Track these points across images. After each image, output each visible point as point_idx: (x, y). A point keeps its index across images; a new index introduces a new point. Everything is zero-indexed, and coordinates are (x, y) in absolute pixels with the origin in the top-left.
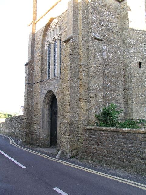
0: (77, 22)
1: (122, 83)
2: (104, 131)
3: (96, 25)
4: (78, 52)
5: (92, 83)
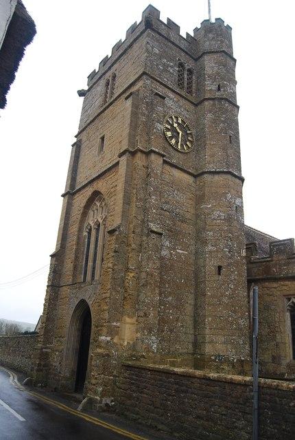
0: (129, 204)
1: (191, 297)
2: (150, 370)
4: (127, 248)
5: (142, 297)
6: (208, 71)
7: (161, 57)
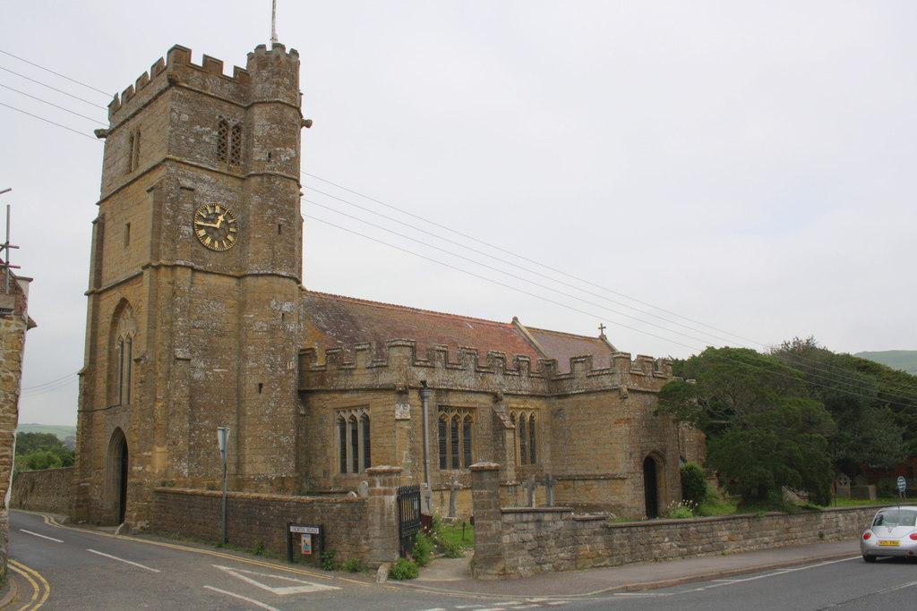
3: (182, 334)
6: (258, 131)
7: (192, 123)
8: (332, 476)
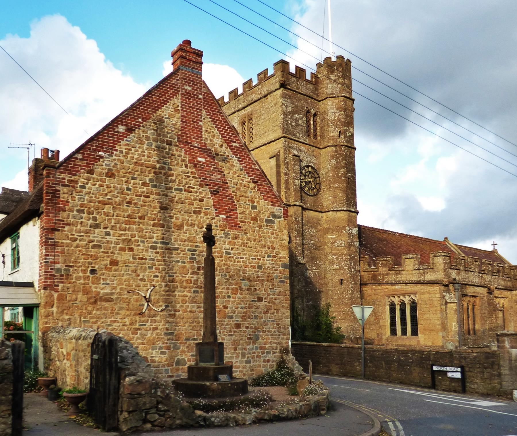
8: (384, 338)
